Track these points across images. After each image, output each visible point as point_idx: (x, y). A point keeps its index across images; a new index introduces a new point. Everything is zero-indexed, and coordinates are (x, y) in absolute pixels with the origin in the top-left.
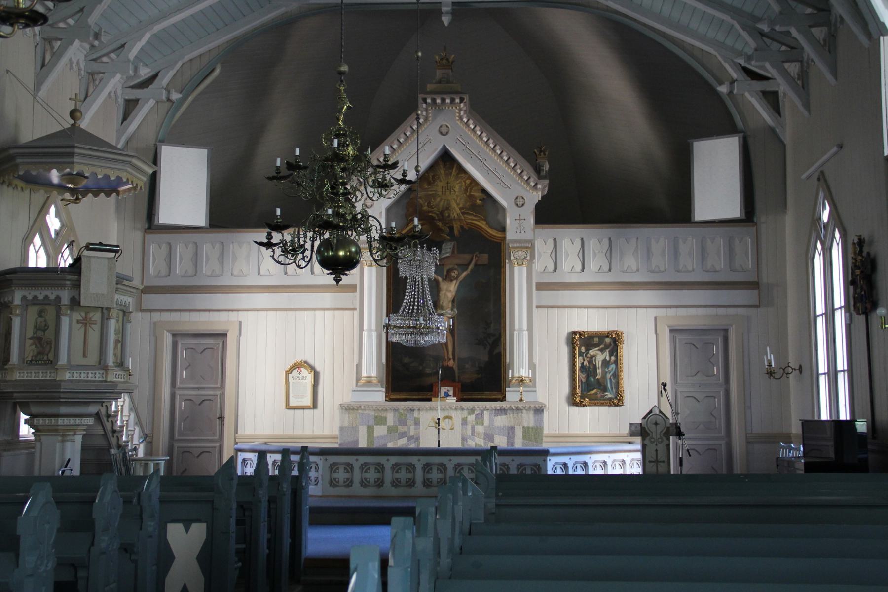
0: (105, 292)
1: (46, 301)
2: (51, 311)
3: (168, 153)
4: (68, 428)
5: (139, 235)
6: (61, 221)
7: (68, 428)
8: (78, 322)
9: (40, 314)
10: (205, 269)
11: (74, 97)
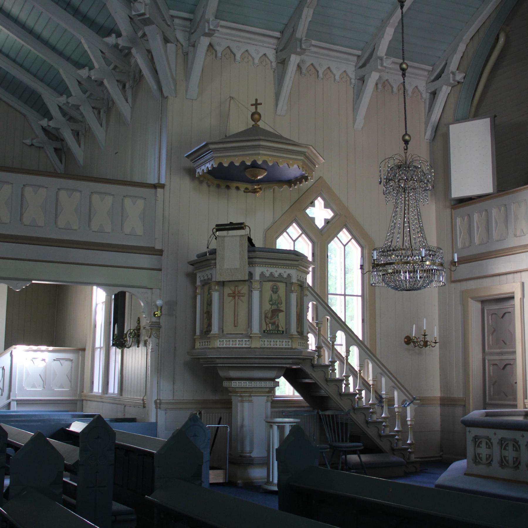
0: (238, 267)
1: (280, 279)
2: (282, 287)
3: (455, 130)
4: (244, 390)
5: (448, 211)
6: (332, 210)
7: (244, 390)
8: (229, 295)
9: (275, 290)
10: (495, 235)
11: (258, 102)
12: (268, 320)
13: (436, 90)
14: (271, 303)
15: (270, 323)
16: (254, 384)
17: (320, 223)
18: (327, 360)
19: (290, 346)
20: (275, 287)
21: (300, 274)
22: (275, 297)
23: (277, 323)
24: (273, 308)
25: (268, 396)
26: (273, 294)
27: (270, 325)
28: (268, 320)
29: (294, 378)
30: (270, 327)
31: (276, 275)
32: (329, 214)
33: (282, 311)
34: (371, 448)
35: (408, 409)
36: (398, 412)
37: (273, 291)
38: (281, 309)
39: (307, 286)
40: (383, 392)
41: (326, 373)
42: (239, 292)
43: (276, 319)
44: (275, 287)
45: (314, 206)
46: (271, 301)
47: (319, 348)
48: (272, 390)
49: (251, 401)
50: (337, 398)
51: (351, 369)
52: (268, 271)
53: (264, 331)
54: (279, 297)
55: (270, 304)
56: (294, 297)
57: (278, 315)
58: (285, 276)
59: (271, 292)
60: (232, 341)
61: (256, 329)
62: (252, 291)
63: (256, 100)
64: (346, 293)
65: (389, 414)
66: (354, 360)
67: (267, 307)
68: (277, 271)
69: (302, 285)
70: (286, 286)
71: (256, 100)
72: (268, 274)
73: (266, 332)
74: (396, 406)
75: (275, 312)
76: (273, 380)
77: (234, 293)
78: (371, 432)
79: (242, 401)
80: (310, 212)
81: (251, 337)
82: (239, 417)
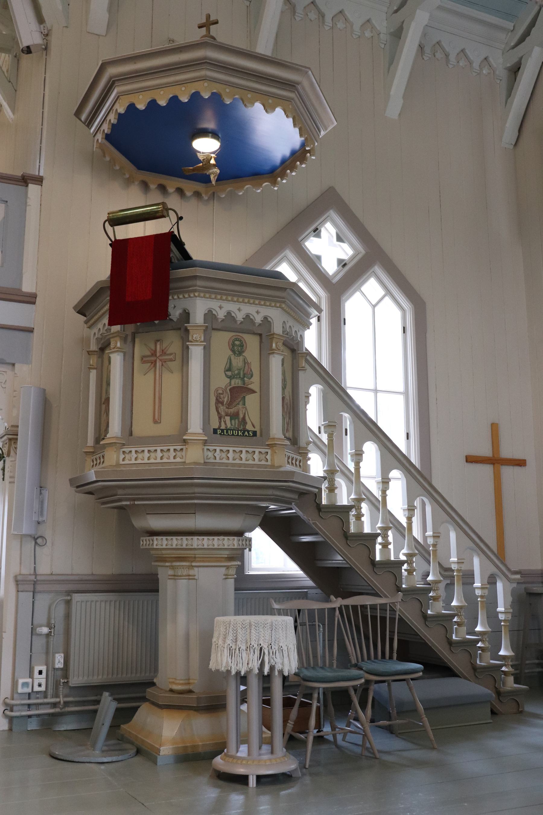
2: (252, 343)
9: (238, 348)
12: (222, 409)
13: (521, 58)
14: (229, 373)
15: (227, 415)
16: (196, 542)
17: (330, 267)
18: (344, 497)
19: (269, 463)
20: (237, 343)
21: (290, 322)
22: (237, 362)
23: (241, 416)
24: (233, 384)
25: (228, 567)
26: (233, 357)
27: (228, 419)
28: (222, 409)
29: (282, 532)
30: (228, 422)
31: (240, 317)
32: (345, 251)
33: (254, 392)
34: (437, 668)
35: (500, 586)
36: (482, 597)
37: (233, 351)
38: (249, 386)
39: (304, 350)
40: (454, 559)
41: (345, 523)
42: (163, 353)
43: (240, 406)
44: (237, 343)
45: (318, 236)
46: (229, 369)
47: (330, 474)
48: (238, 556)
49: (190, 577)
50: (364, 570)
51: (390, 518)
52: (222, 308)
53: (215, 431)
54: (245, 362)
55: (227, 376)
56: (276, 363)
57: (244, 398)
58: (258, 319)
59: (231, 353)
60: (149, 451)
61: (195, 424)
62: (188, 348)
63: (208, 16)
64: (378, 389)
65: (466, 600)
66: (397, 501)
67: (221, 381)
68: (241, 310)
69: (294, 348)
70: (261, 342)
71: (208, 16)
72: (221, 315)
73: (219, 432)
74: (477, 584)
75: (238, 393)
76: (240, 534)
77: (154, 354)
78: (432, 637)
79: (175, 577)
80: (313, 245)
81: (185, 442)
82: (318, 651)
